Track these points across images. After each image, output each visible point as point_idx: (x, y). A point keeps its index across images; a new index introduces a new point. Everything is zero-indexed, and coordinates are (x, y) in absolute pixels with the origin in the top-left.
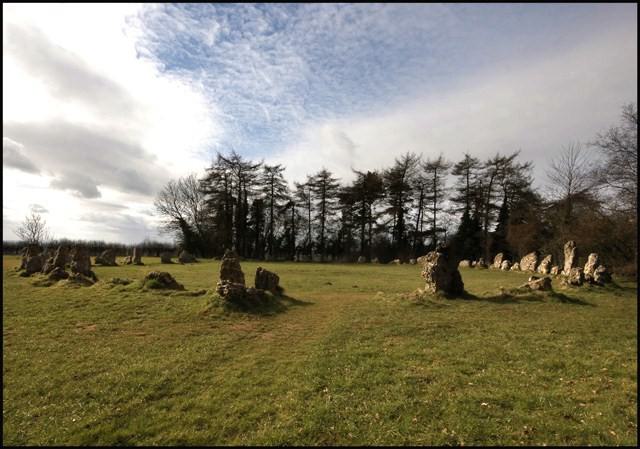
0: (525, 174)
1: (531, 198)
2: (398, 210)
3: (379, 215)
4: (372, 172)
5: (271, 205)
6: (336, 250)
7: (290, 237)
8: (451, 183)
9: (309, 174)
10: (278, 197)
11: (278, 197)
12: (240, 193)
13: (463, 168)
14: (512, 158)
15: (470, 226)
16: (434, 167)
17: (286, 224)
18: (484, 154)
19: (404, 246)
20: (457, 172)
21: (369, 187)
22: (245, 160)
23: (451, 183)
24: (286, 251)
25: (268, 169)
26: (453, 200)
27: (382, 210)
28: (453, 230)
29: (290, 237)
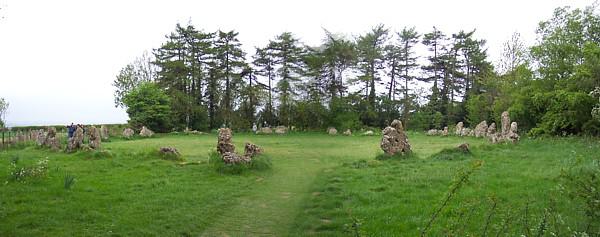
0: (482, 49)
1: (487, 67)
2: (370, 78)
3: (350, 81)
4: (364, 36)
5: (227, 74)
6: (307, 120)
7: (248, 110)
8: (421, 53)
9: (333, 32)
10: (234, 64)
11: (234, 64)
12: (193, 61)
13: (430, 39)
14: (470, 34)
15: (440, 99)
16: (407, 36)
17: (243, 93)
18: (450, 29)
19: (371, 115)
20: (426, 42)
21: (338, 53)
22: (466, 32)
23: (421, 53)
24: (245, 121)
25: (222, 35)
26: (423, 68)
27: (353, 76)
28: (423, 102)
29: (248, 110)
